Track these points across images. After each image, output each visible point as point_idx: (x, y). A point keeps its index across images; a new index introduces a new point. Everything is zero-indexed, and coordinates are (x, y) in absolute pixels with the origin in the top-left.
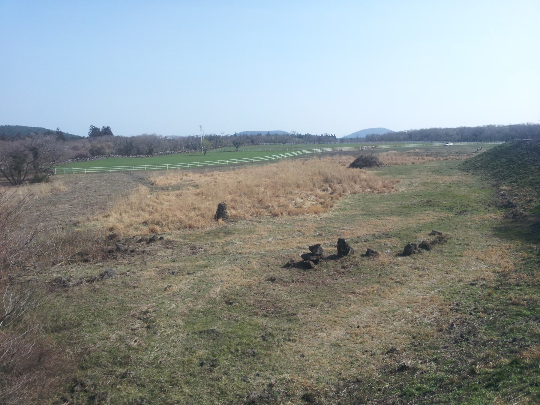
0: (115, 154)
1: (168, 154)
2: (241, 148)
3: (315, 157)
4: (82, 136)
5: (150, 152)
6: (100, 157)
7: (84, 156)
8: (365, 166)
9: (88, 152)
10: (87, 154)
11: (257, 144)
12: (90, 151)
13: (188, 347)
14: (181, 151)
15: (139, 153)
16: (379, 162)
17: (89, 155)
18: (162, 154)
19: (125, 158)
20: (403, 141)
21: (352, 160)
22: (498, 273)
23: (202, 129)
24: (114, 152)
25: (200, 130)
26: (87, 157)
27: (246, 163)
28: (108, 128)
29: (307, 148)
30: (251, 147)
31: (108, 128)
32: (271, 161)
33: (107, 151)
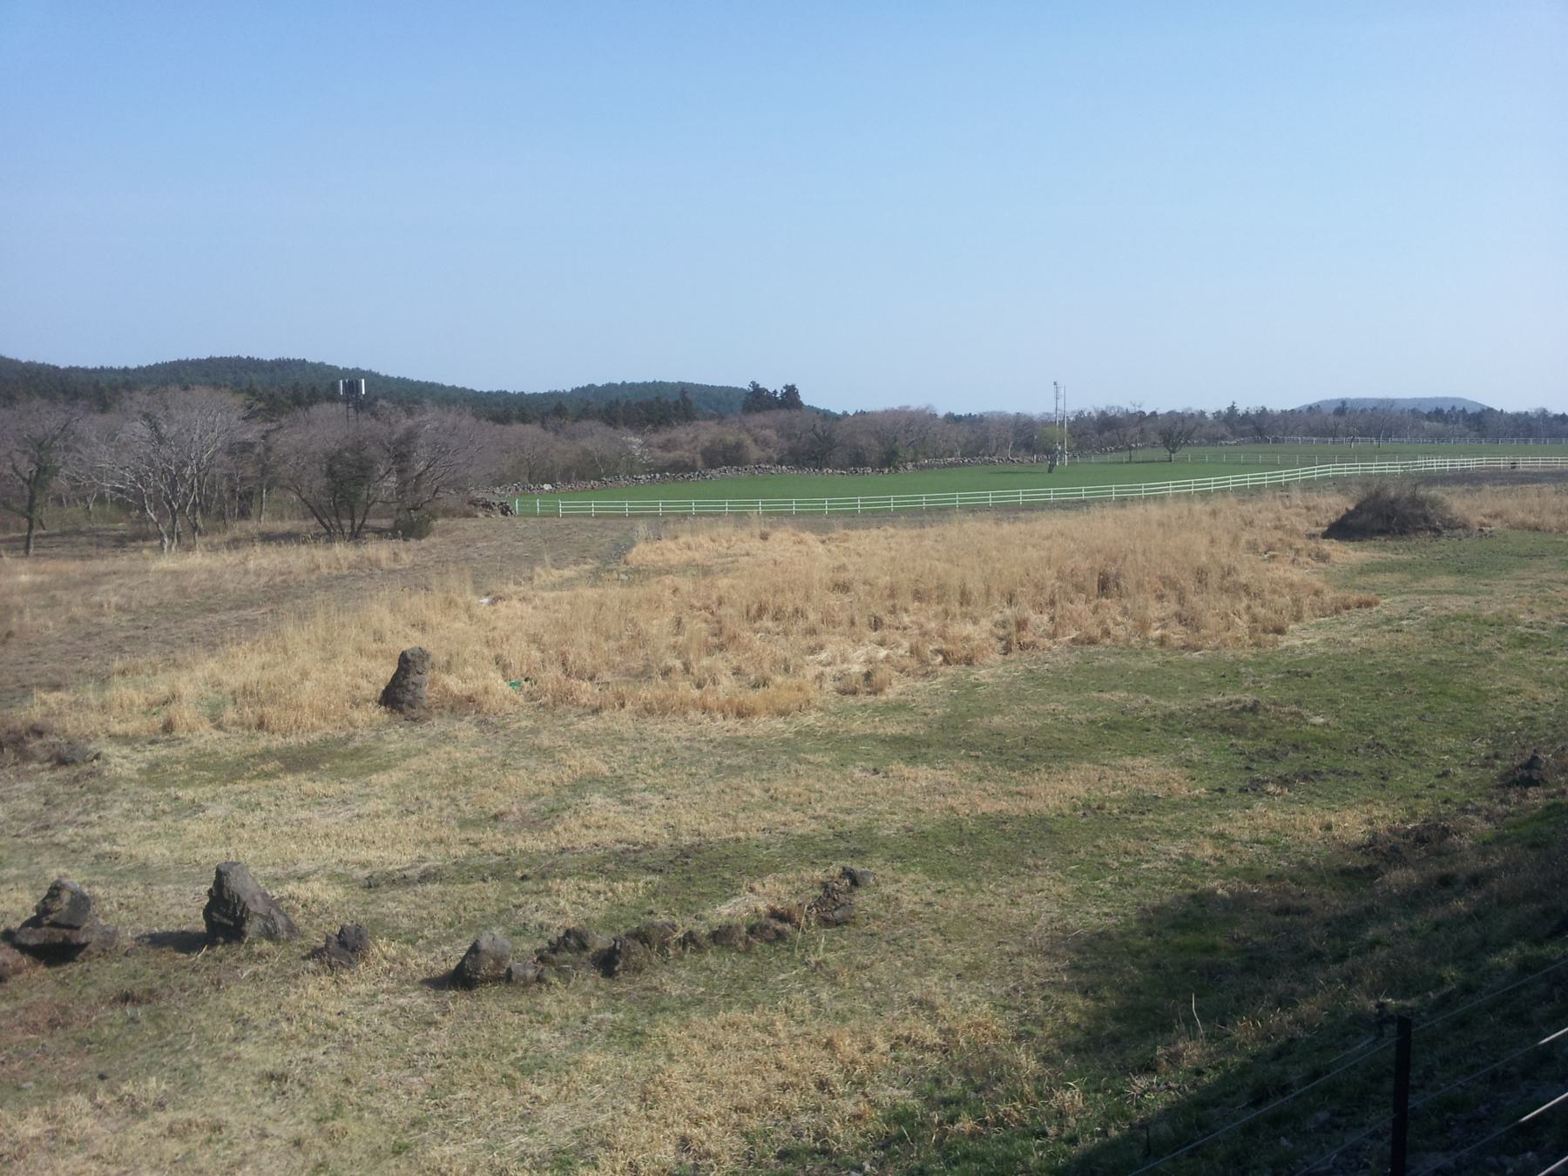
0: (780, 463)
1: (951, 465)
2: (1184, 452)
3: (1269, 496)
4: (839, 412)
5: (889, 460)
6: (731, 472)
7: (686, 465)
8: (1382, 532)
9: (698, 457)
10: (694, 461)
11: (1276, 441)
12: (703, 453)
13: (393, 1162)
14: (995, 459)
15: (857, 461)
16: (1442, 519)
17: (700, 463)
18: (930, 466)
19: (809, 476)
20: (567, 479)
21: (1336, 504)
22: (1024, 1126)
23: (1062, 392)
24: (775, 457)
25: (1053, 396)
26: (693, 469)
27: (1084, 501)
28: (793, 386)
29: (1363, 457)
30: (1255, 447)
31: (793, 386)
32: (1065, 506)
33: (754, 452)
